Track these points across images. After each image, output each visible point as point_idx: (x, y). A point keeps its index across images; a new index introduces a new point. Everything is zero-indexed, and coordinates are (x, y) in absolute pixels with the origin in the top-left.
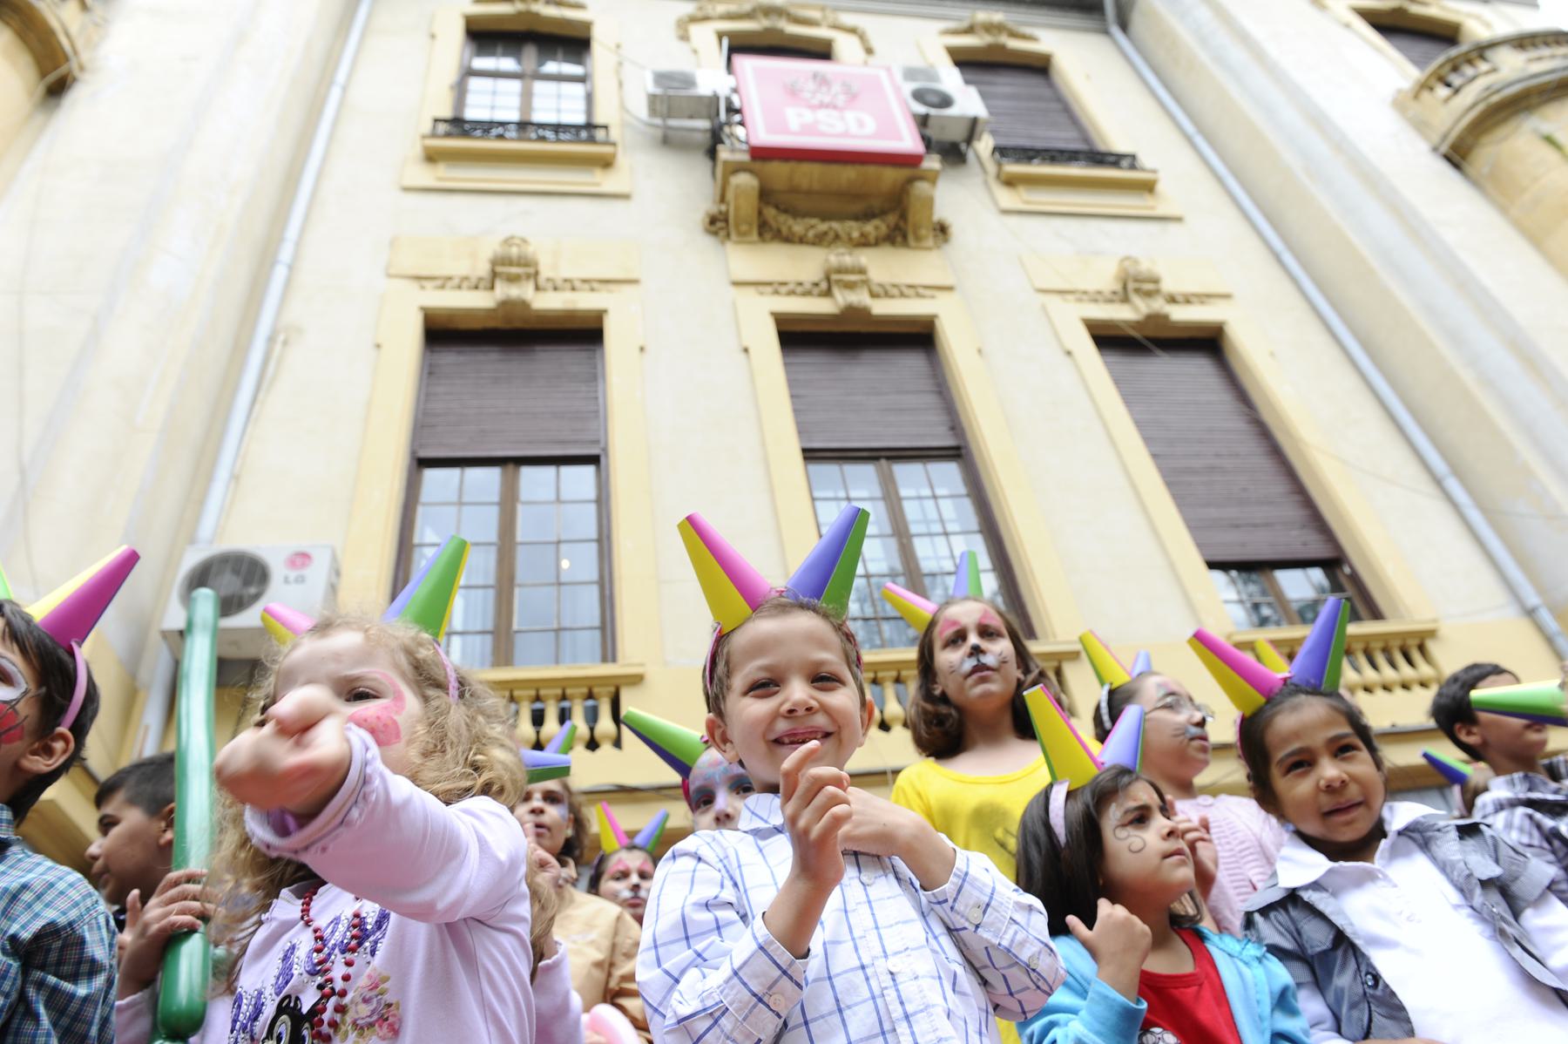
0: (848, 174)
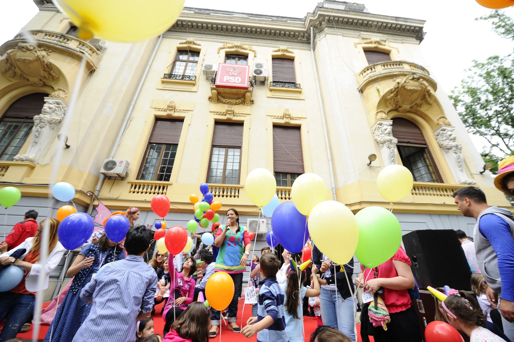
0: (234, 90)
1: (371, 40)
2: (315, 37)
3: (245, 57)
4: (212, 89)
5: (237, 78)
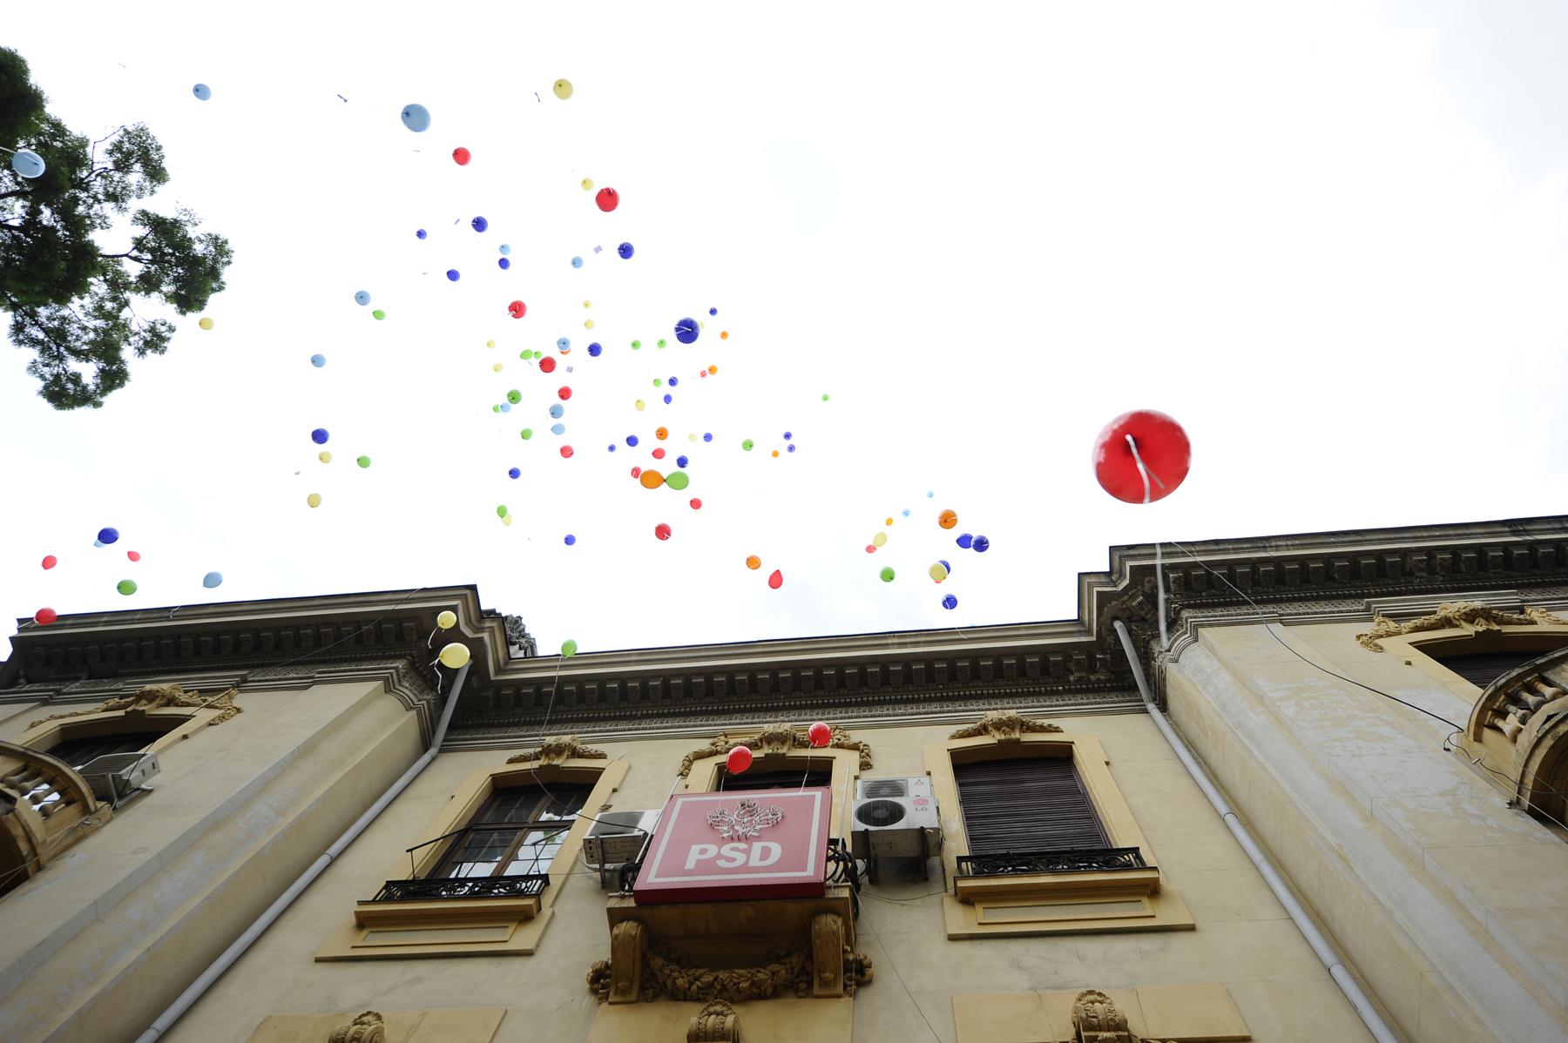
0: (746, 911)
1: (1442, 613)
2: (1146, 657)
3: (820, 775)
4: (615, 917)
5: (757, 847)
